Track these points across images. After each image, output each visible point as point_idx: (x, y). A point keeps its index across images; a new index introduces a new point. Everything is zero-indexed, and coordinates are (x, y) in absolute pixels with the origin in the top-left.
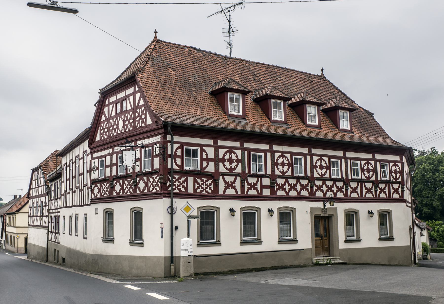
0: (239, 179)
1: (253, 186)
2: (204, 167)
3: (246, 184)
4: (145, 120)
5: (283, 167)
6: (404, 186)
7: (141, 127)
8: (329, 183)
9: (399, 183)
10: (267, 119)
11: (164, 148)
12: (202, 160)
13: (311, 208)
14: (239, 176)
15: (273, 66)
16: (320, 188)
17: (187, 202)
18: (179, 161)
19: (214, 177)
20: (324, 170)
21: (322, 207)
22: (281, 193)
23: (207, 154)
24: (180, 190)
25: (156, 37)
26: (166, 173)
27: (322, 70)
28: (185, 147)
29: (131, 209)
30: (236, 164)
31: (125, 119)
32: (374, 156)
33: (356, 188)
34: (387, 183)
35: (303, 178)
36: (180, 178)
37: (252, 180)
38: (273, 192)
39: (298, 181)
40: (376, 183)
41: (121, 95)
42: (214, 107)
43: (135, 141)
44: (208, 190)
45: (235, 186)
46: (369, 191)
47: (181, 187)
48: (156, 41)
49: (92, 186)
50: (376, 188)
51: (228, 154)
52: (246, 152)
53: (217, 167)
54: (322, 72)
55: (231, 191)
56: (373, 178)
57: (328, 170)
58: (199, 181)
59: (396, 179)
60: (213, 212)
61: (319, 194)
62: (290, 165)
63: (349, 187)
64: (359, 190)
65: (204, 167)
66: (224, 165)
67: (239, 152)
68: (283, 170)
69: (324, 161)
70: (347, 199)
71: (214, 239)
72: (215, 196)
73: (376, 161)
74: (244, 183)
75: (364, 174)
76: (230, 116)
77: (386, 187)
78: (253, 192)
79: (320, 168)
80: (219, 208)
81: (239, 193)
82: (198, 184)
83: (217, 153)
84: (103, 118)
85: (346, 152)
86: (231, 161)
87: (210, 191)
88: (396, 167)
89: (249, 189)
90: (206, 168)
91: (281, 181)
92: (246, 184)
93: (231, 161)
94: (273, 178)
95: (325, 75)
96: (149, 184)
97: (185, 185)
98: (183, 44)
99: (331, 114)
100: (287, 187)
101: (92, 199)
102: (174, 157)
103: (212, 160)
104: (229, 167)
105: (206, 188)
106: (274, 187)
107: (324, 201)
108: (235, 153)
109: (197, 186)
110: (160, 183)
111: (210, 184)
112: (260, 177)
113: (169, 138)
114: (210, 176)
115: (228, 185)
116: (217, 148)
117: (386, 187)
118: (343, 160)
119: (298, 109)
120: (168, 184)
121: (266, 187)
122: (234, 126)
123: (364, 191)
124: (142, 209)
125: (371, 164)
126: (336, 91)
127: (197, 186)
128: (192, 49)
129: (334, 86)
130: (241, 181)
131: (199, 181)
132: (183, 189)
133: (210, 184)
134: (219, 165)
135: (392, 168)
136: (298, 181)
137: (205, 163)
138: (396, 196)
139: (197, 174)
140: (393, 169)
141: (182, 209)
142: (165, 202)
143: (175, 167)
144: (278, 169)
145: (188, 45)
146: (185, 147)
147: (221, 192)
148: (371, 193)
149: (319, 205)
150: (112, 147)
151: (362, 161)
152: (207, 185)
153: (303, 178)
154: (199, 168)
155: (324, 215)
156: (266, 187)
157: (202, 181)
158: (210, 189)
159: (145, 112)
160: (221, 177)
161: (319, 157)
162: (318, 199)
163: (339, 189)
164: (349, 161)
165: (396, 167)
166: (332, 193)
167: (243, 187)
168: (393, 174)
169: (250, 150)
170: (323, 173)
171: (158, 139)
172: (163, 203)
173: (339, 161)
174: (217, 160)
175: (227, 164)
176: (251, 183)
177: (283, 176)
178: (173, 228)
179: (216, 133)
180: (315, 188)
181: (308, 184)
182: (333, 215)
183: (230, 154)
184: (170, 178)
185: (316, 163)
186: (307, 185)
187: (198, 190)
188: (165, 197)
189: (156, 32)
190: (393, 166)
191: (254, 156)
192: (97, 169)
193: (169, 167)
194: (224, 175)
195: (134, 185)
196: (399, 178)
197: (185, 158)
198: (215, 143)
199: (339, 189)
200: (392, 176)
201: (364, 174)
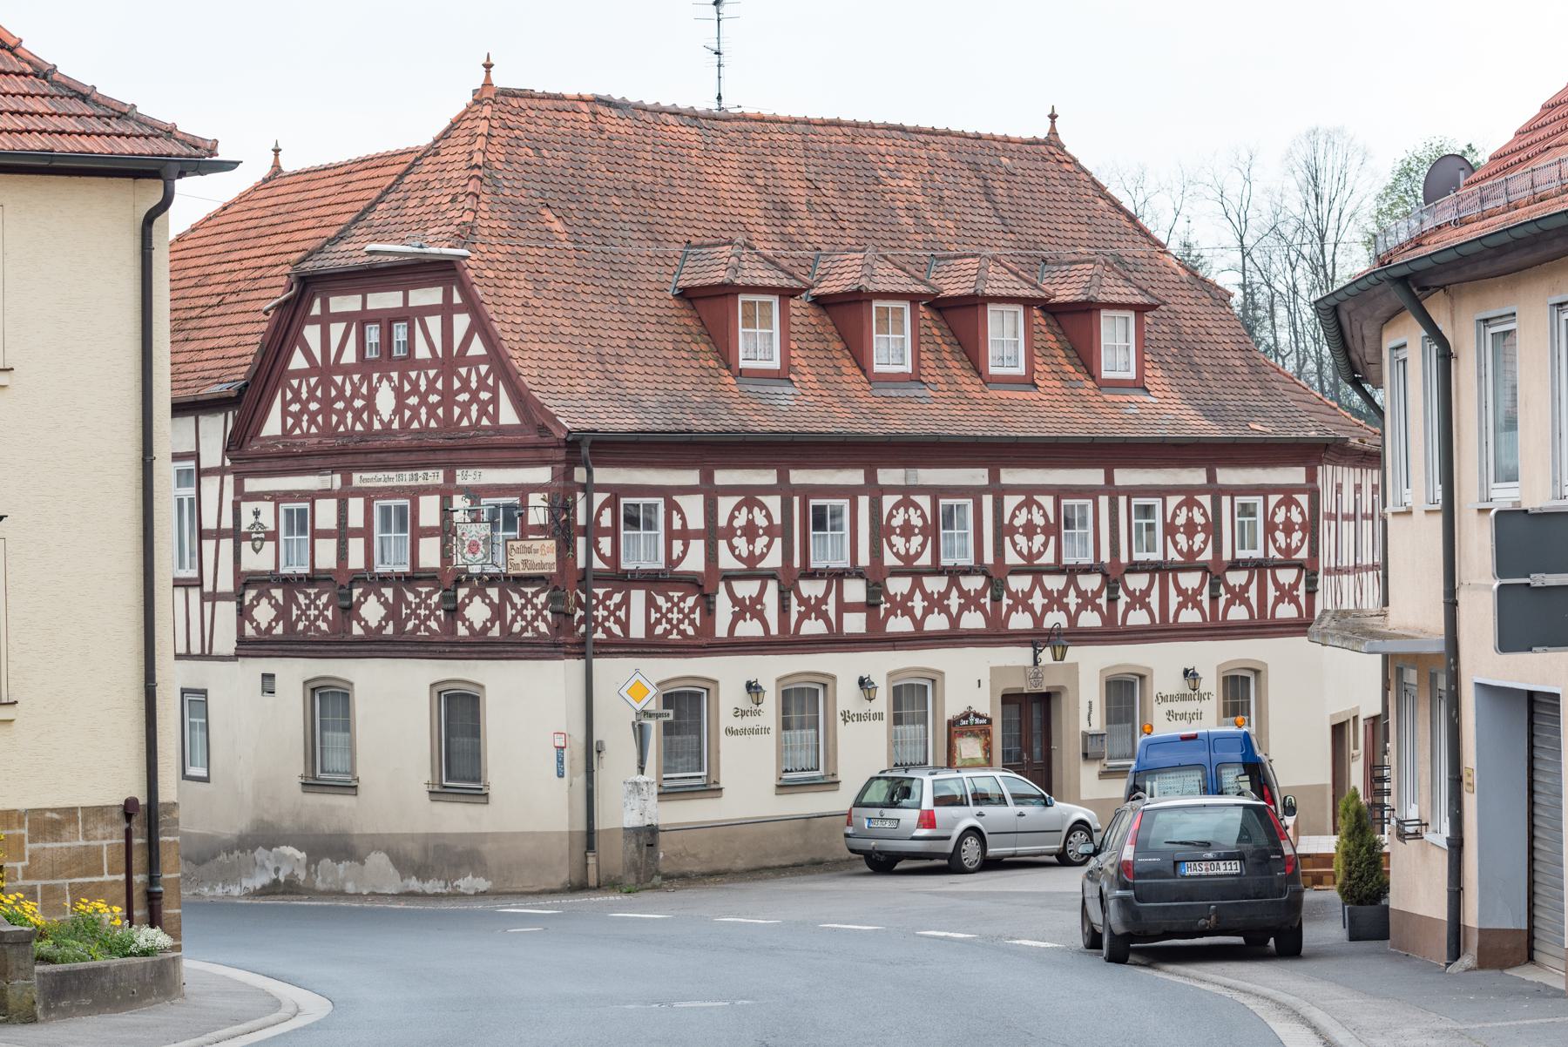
0: (772, 586)
1: (814, 608)
2: (675, 557)
3: (794, 601)
4: (491, 409)
5: (908, 541)
6: (1316, 573)
7: (475, 426)
8: (1054, 583)
9: (1300, 566)
10: (857, 371)
11: (561, 506)
12: (670, 535)
14: (773, 577)
15: (873, 126)
16: (1022, 602)
17: (637, 671)
18: (605, 544)
19: (702, 587)
20: (1039, 539)
21: (1030, 662)
22: (899, 625)
23: (683, 518)
24: (607, 631)
26: (567, 585)
27: (1053, 117)
28: (623, 501)
29: (432, 685)
30: (765, 539)
31: (407, 387)
32: (1212, 477)
33: (1147, 593)
35: (967, 572)
36: (608, 596)
38: (875, 623)
39: (954, 582)
40: (1214, 573)
41: (388, 300)
42: (693, 346)
43: (450, 468)
44: (685, 626)
45: (762, 611)
46: (1190, 599)
47: (610, 624)
48: (1053, 140)
49: (242, 595)
50: (1214, 588)
52: (796, 500)
54: (1053, 122)
55: (749, 629)
56: (1207, 556)
57: (1052, 539)
58: (660, 600)
59: (1288, 551)
60: (700, 695)
61: (1020, 621)
62: (931, 531)
63: (1121, 592)
64: (1154, 600)
65: (675, 557)
67: (774, 503)
69: (1040, 507)
70: (1112, 633)
71: (700, 769)
73: (1217, 492)
74: (789, 599)
75: (1175, 544)
76: (741, 373)
77: (1249, 581)
79: (1023, 534)
80: (715, 682)
81: (774, 631)
82: (658, 609)
83: (711, 512)
84: (298, 361)
86: (750, 532)
87: (690, 631)
88: (1288, 510)
89: (802, 617)
90: (680, 559)
91: (898, 586)
92: (794, 601)
93: (750, 532)
94: (875, 578)
95: (1063, 138)
96: (510, 613)
97: (622, 614)
98: (570, 91)
99: (1069, 324)
100: (918, 604)
101: (242, 641)
102: (592, 531)
103: (697, 534)
105: (680, 621)
106: (877, 606)
107: (1034, 645)
108: (762, 506)
109: (654, 616)
110: (553, 612)
111: (692, 610)
112: (837, 576)
113: (580, 475)
114: (691, 583)
115: (745, 608)
116: (711, 493)
117: (1249, 581)
118: (1104, 501)
119: (955, 318)
120: (576, 617)
121: (854, 608)
123: (1174, 600)
124: (482, 687)
125: (1200, 506)
126: (1101, 203)
127: (654, 616)
128: (600, 109)
129: (1093, 180)
130: (781, 592)
131: (660, 600)
132: (616, 630)
133: (692, 610)
135: (1274, 513)
136: (954, 582)
137: (677, 546)
138: (1286, 611)
139: (650, 580)
140: (1280, 518)
141: (623, 692)
142: (567, 671)
143: (598, 564)
144: (891, 546)
145: (587, 92)
146: (623, 501)
147: (721, 631)
148: (1198, 605)
149: (1020, 656)
150: (346, 472)
151: (1169, 499)
152: (681, 609)
154: (660, 564)
155: (1033, 689)
156: (854, 608)
157: (669, 599)
158: (692, 623)
159: (490, 381)
160: (722, 586)
161: (1022, 498)
162: (1018, 638)
163: (1087, 601)
164: (1122, 500)
165: (1288, 510)
167: (784, 609)
168: (1280, 536)
169: (808, 492)
170: (1035, 550)
171: (543, 475)
172: (556, 678)
173: (1089, 502)
174: (712, 534)
175: (741, 543)
178: (592, 750)
179: (705, 450)
180: (1006, 601)
181: (984, 589)
182: (1062, 688)
183: (750, 511)
184: (583, 597)
185: (1014, 516)
186: (981, 593)
187: (659, 630)
188: (568, 655)
190: (1278, 505)
191: (820, 510)
192: (273, 536)
193: (581, 564)
194: (729, 577)
195: (447, 611)
196: (1298, 549)
197: (622, 532)
198: (707, 477)
199: (1087, 601)
200: (1275, 541)
201: (1175, 544)
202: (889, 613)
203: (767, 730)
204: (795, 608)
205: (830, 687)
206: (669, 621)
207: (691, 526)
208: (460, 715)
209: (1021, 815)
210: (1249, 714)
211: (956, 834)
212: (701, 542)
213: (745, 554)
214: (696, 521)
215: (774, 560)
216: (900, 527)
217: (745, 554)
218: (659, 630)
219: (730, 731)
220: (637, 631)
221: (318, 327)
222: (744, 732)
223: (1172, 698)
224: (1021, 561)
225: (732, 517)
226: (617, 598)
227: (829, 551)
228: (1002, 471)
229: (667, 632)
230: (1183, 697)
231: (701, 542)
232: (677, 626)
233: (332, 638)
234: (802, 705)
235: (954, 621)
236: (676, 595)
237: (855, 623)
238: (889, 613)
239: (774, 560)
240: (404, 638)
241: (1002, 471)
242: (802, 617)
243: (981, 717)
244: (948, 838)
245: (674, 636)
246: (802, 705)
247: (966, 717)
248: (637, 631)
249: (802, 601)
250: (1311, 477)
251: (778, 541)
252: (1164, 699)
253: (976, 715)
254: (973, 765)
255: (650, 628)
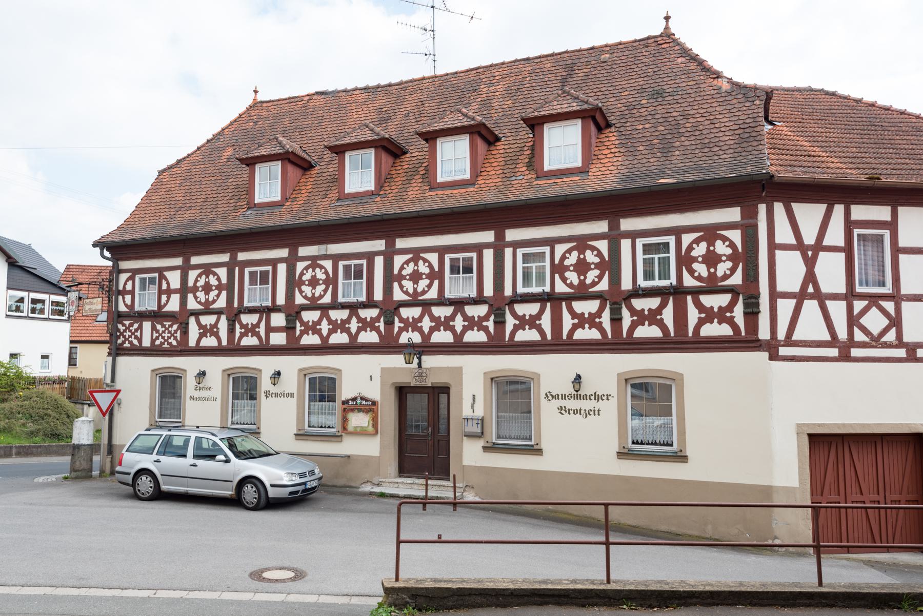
0: (223, 319)
1: (252, 330)
3: (237, 326)
12: (161, 292)
13: (461, 368)
19: (181, 318)
22: (311, 339)
23: (168, 283)
25: (667, 28)
34: (549, 300)
36: (131, 325)
37: (249, 319)
45: (217, 332)
48: (667, 34)
51: (204, 277)
53: (183, 302)
55: (209, 342)
57: (436, 282)
58: (159, 327)
66: (196, 298)
68: (313, 294)
70: (498, 345)
72: (183, 350)
78: (250, 341)
81: (224, 343)
82: (157, 331)
83: (184, 279)
85: (853, 207)
86: (207, 288)
87: (174, 343)
89: (242, 335)
90: (165, 305)
103: (175, 291)
104: (309, 295)
106: (295, 328)
108: (215, 274)
111: (176, 332)
114: (171, 316)
115: (205, 331)
116: (185, 270)
121: (278, 330)
122: (268, 221)
131: (159, 327)
132: (136, 342)
133: (176, 332)
134: (186, 297)
139: (157, 316)
144: (301, 292)
147: (192, 343)
149: (396, 361)
152: (170, 334)
153: (365, 306)
156: (278, 330)
157: (163, 326)
158: (175, 338)
166: (345, 335)
167: (231, 331)
175: (201, 295)
176: (247, 324)
177: (313, 305)
187: (158, 342)
189: (667, 18)
194: (196, 314)
202: (303, 333)
203: (215, 399)
204: (238, 330)
205: (305, 372)
206: (163, 338)
207: (172, 287)
208: (169, 386)
209: (195, 465)
210: (671, 415)
211: (133, 471)
212: (178, 296)
213: (203, 300)
214: (175, 283)
215: (221, 303)
216: (308, 280)
217: (203, 300)
218: (158, 342)
219: (192, 398)
220: (146, 343)
221: (630, 240)
222: (200, 399)
223: (564, 397)
224: (407, 298)
225: (196, 281)
226: (136, 326)
227: (255, 296)
228: (397, 240)
229: (162, 343)
230: (570, 397)
231: (178, 296)
232: (167, 341)
233: (179, 349)
234: (245, 388)
235: (354, 338)
236: (167, 324)
237: (278, 339)
238: (303, 333)
239: (221, 303)
240: (155, 348)
241: (397, 240)
242: (242, 335)
243: (366, 400)
244: (129, 474)
245: (166, 345)
246: (245, 388)
247: (355, 399)
248: (146, 343)
249: (242, 326)
250: (894, 215)
251: (224, 293)
252: (555, 397)
253: (362, 399)
254: (361, 433)
255: (153, 341)
